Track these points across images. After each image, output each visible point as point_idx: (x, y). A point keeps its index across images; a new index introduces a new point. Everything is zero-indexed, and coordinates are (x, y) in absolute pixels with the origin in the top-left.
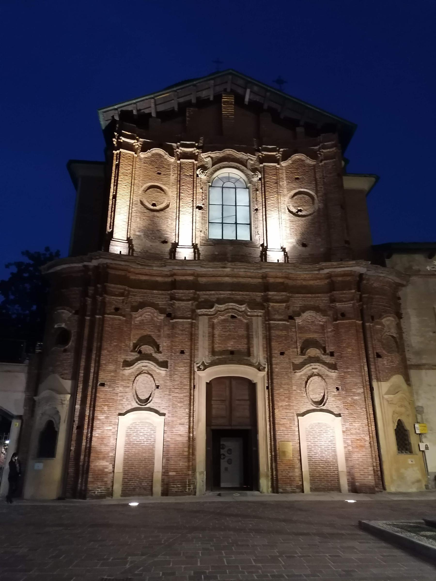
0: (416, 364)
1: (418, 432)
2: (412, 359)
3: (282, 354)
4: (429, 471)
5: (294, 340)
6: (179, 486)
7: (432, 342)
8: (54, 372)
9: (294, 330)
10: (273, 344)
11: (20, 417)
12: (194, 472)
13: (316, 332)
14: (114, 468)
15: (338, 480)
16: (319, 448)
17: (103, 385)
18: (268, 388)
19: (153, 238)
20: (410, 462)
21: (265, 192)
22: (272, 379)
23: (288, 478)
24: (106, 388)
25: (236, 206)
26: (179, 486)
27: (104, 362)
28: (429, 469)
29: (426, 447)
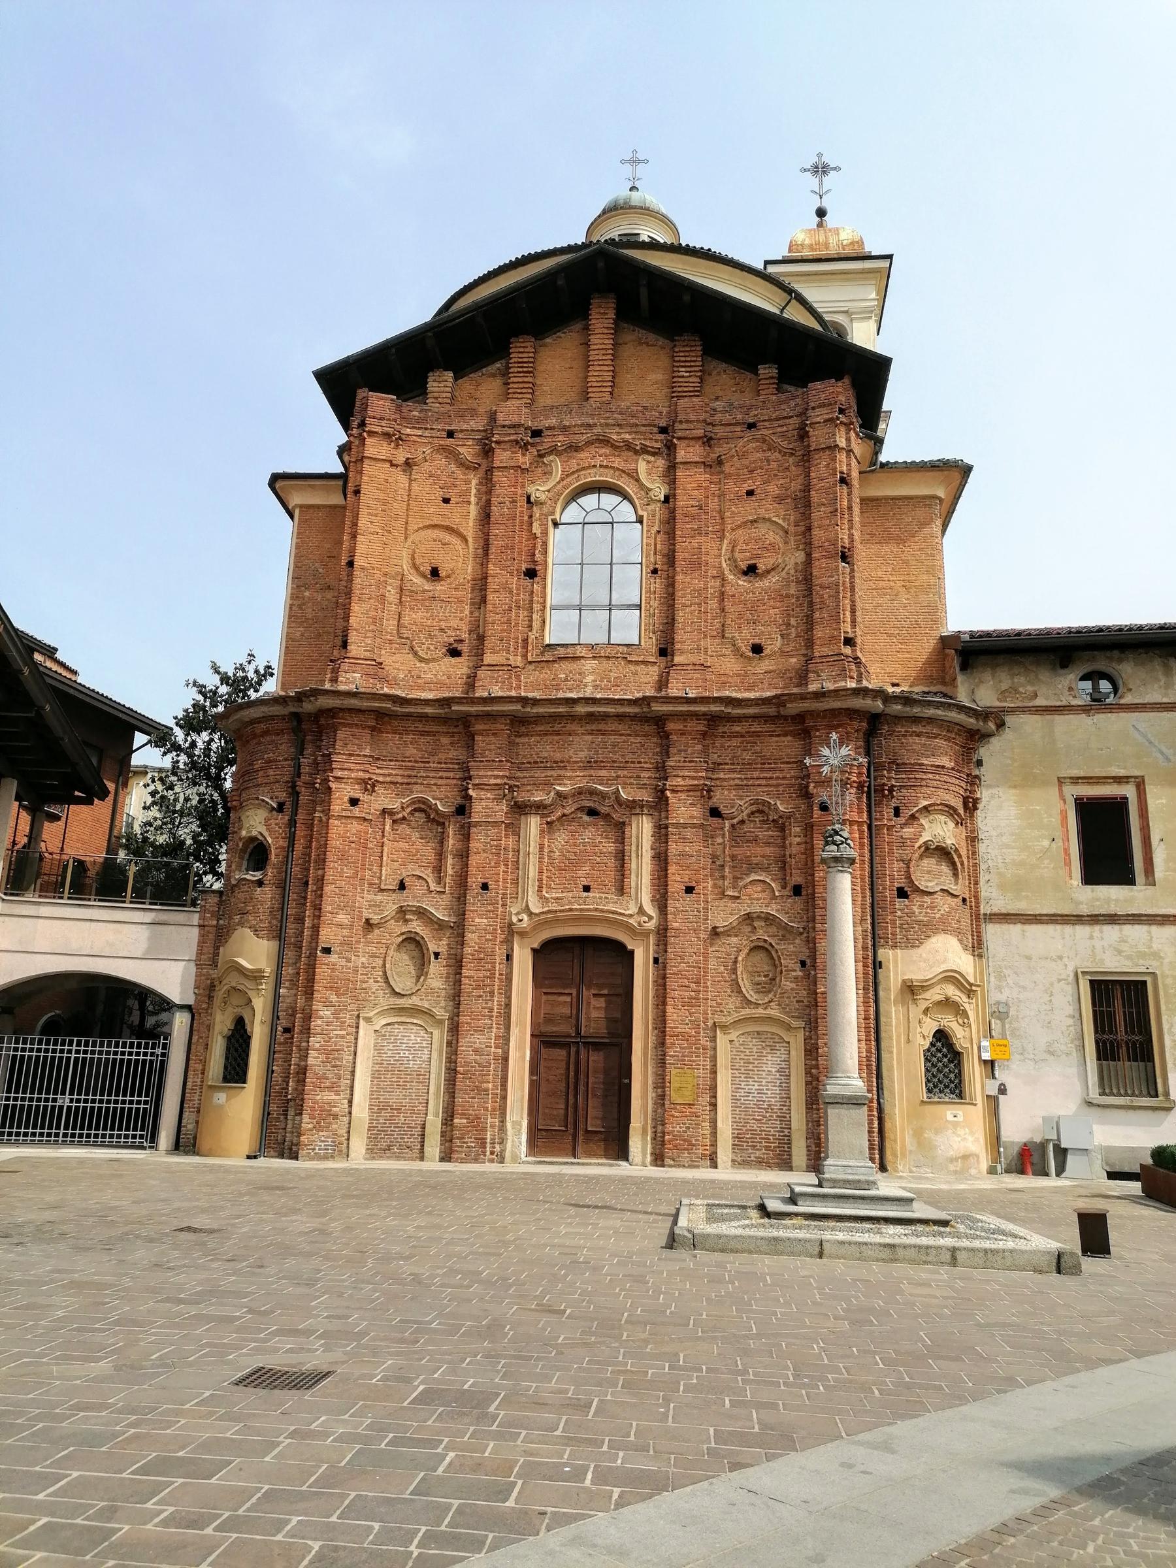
0: (1004, 911)
1: (986, 1056)
2: (994, 899)
3: (689, 890)
4: (1003, 1139)
5: (718, 863)
6: (473, 1145)
7: (1046, 862)
8: (241, 924)
9: (719, 840)
10: (672, 869)
11: (188, 1008)
12: (502, 1122)
13: (768, 844)
14: (350, 1106)
15: (789, 1148)
16: (756, 1084)
17: (327, 951)
18: (656, 961)
19: (432, 648)
20: (950, 1117)
21: (281, 927)
22: (458, 1005)
23: (685, 1140)
24: (333, 958)
25: (611, 564)
26: (473, 1145)
27: (329, 908)
28: (1003, 1133)
29: (999, 1090)
